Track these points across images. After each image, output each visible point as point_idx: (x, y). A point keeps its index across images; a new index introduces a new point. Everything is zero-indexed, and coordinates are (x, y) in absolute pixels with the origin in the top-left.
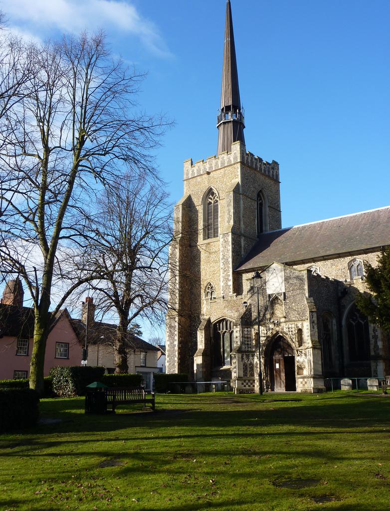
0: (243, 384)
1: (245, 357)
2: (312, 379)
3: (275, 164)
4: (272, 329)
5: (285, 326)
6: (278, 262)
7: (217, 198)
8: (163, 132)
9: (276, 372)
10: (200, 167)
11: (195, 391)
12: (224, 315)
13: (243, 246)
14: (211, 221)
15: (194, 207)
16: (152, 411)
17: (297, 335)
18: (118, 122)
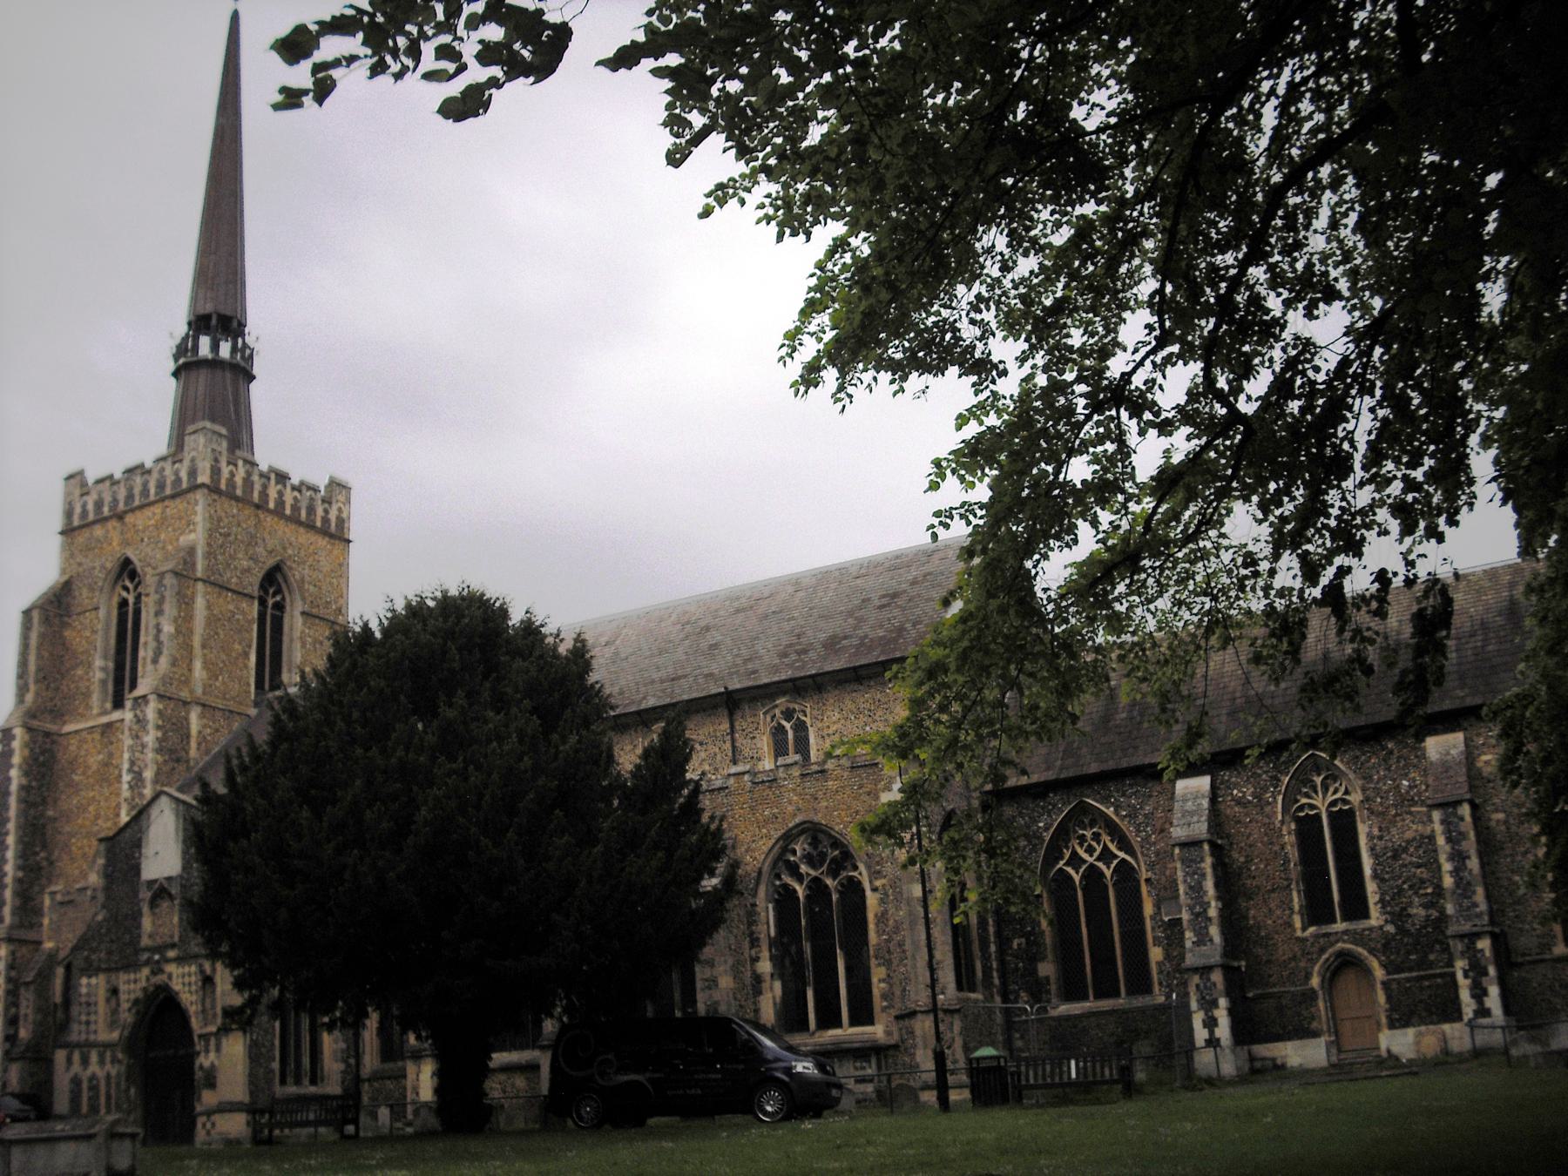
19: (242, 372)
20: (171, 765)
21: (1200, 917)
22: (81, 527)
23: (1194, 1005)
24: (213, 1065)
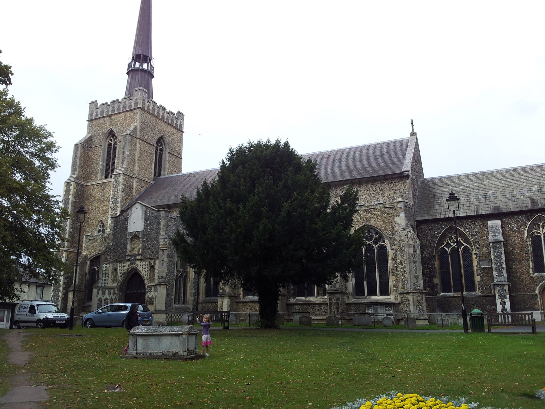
13: (135, 187)
19: (150, 74)
20: (127, 197)
21: (499, 267)
22: (95, 119)
23: (497, 297)
24: (152, 297)
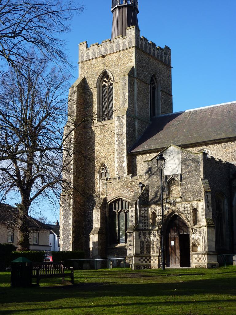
0: (140, 260)
1: (142, 235)
2: (206, 256)
3: (168, 49)
4: (169, 208)
5: (181, 205)
6: (174, 143)
7: (112, 81)
8: (71, 16)
9: (171, 249)
10: (95, 50)
11: (92, 267)
12: (120, 195)
13: (137, 129)
14: (105, 104)
15: (89, 89)
16: (70, 284)
17: (192, 214)
18: (29, 6)
